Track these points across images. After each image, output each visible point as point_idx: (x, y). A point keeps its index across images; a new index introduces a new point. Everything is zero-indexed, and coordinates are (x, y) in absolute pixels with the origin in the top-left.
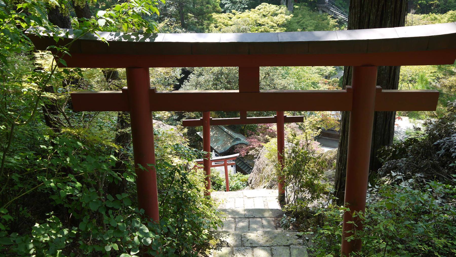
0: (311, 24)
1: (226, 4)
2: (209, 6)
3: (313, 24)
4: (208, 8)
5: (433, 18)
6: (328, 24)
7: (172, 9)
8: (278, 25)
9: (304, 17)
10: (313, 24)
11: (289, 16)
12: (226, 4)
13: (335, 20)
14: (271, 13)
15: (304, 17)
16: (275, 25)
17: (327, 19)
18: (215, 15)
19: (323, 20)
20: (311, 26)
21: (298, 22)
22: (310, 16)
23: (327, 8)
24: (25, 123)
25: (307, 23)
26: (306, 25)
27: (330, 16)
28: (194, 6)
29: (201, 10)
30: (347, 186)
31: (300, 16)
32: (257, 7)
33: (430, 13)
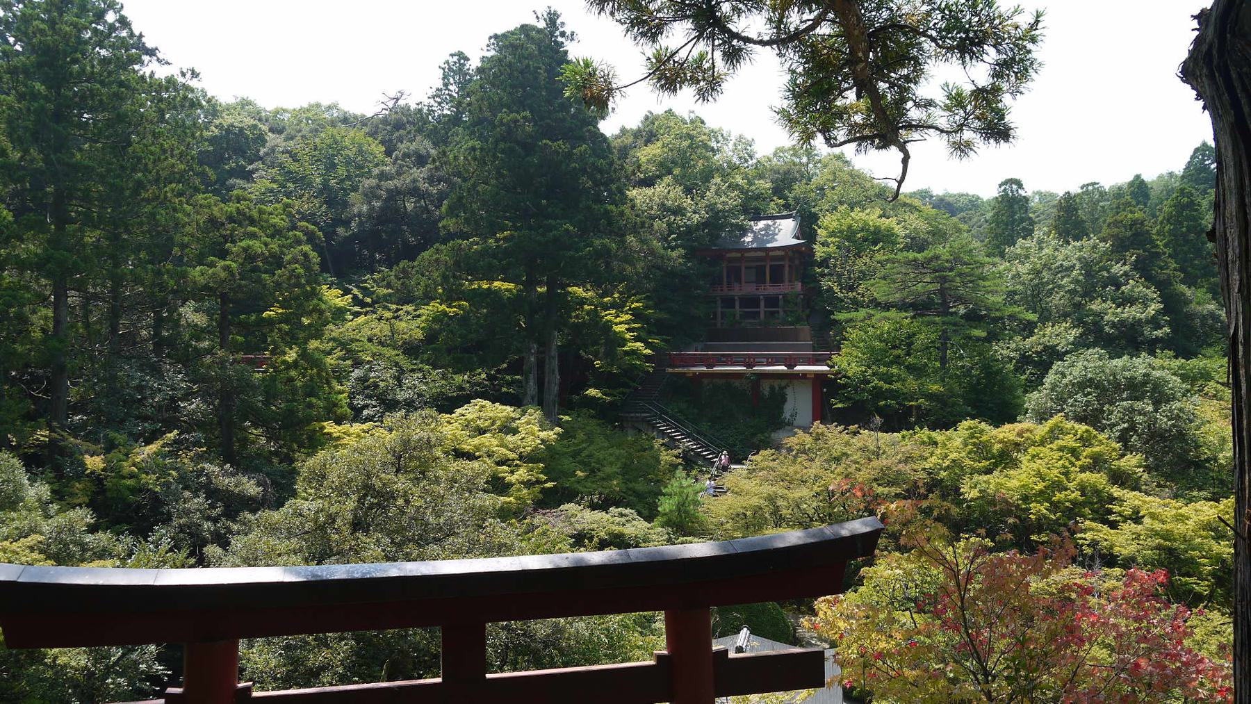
0: (612, 459)
1: (366, 407)
2: (314, 400)
3: (618, 458)
4: (310, 406)
5: (926, 439)
6: (658, 461)
7: (194, 406)
8: (521, 458)
9: (590, 439)
10: (618, 458)
11: (551, 433)
12: (366, 407)
13: (675, 452)
14: (498, 423)
15: (590, 439)
16: (512, 455)
17: (652, 448)
18: (330, 428)
19: (644, 450)
20: (611, 464)
21: (575, 455)
22: (607, 437)
23: (648, 423)
24: (1011, 520)
25: (600, 455)
26: (598, 461)
27: (661, 441)
28: (267, 403)
29: (291, 412)
30: (400, 687)
31: (581, 436)
32: (459, 411)
33: (917, 428)
